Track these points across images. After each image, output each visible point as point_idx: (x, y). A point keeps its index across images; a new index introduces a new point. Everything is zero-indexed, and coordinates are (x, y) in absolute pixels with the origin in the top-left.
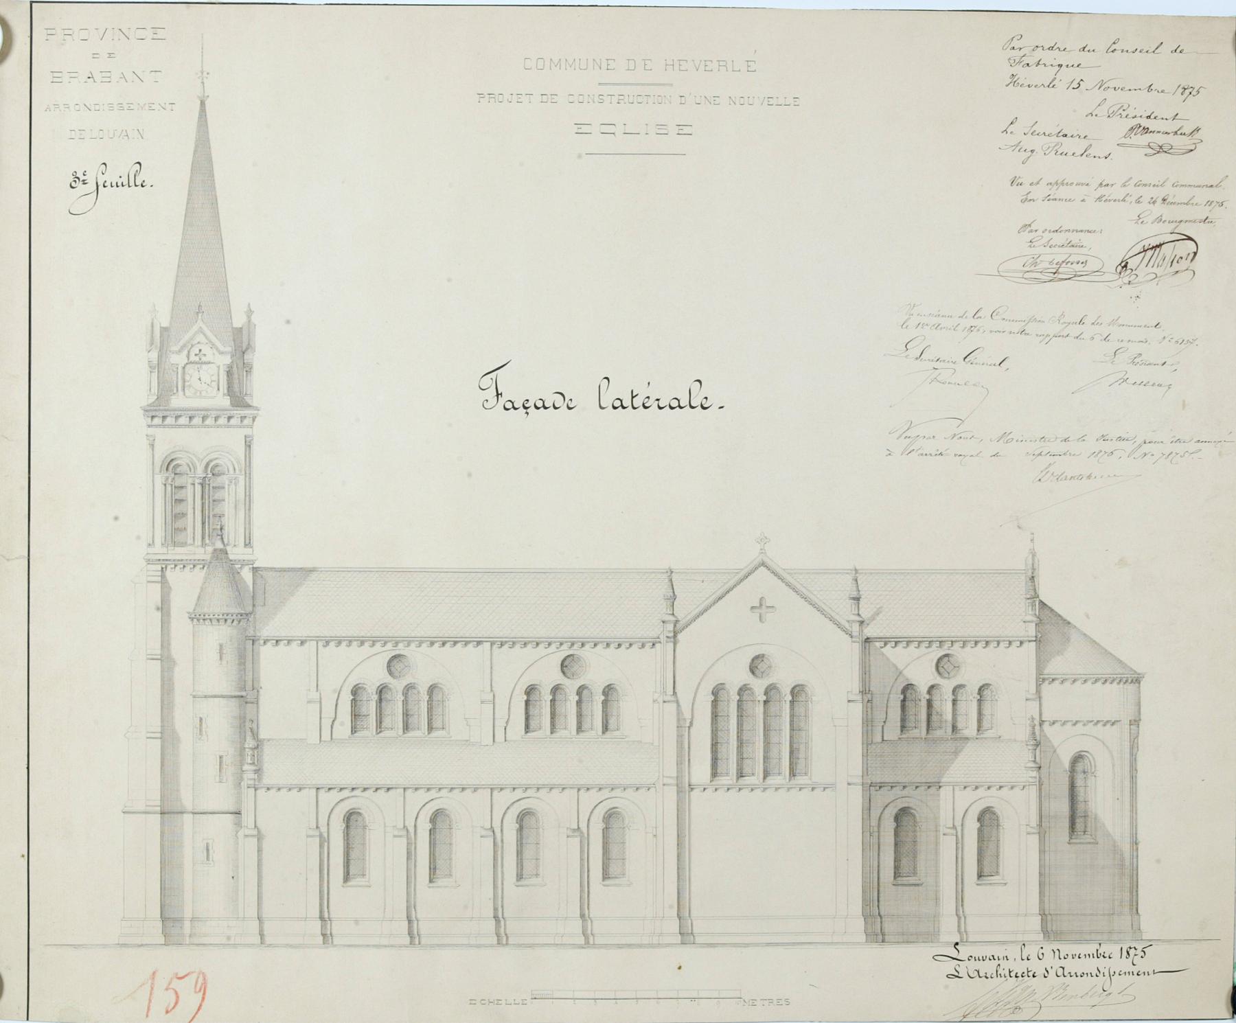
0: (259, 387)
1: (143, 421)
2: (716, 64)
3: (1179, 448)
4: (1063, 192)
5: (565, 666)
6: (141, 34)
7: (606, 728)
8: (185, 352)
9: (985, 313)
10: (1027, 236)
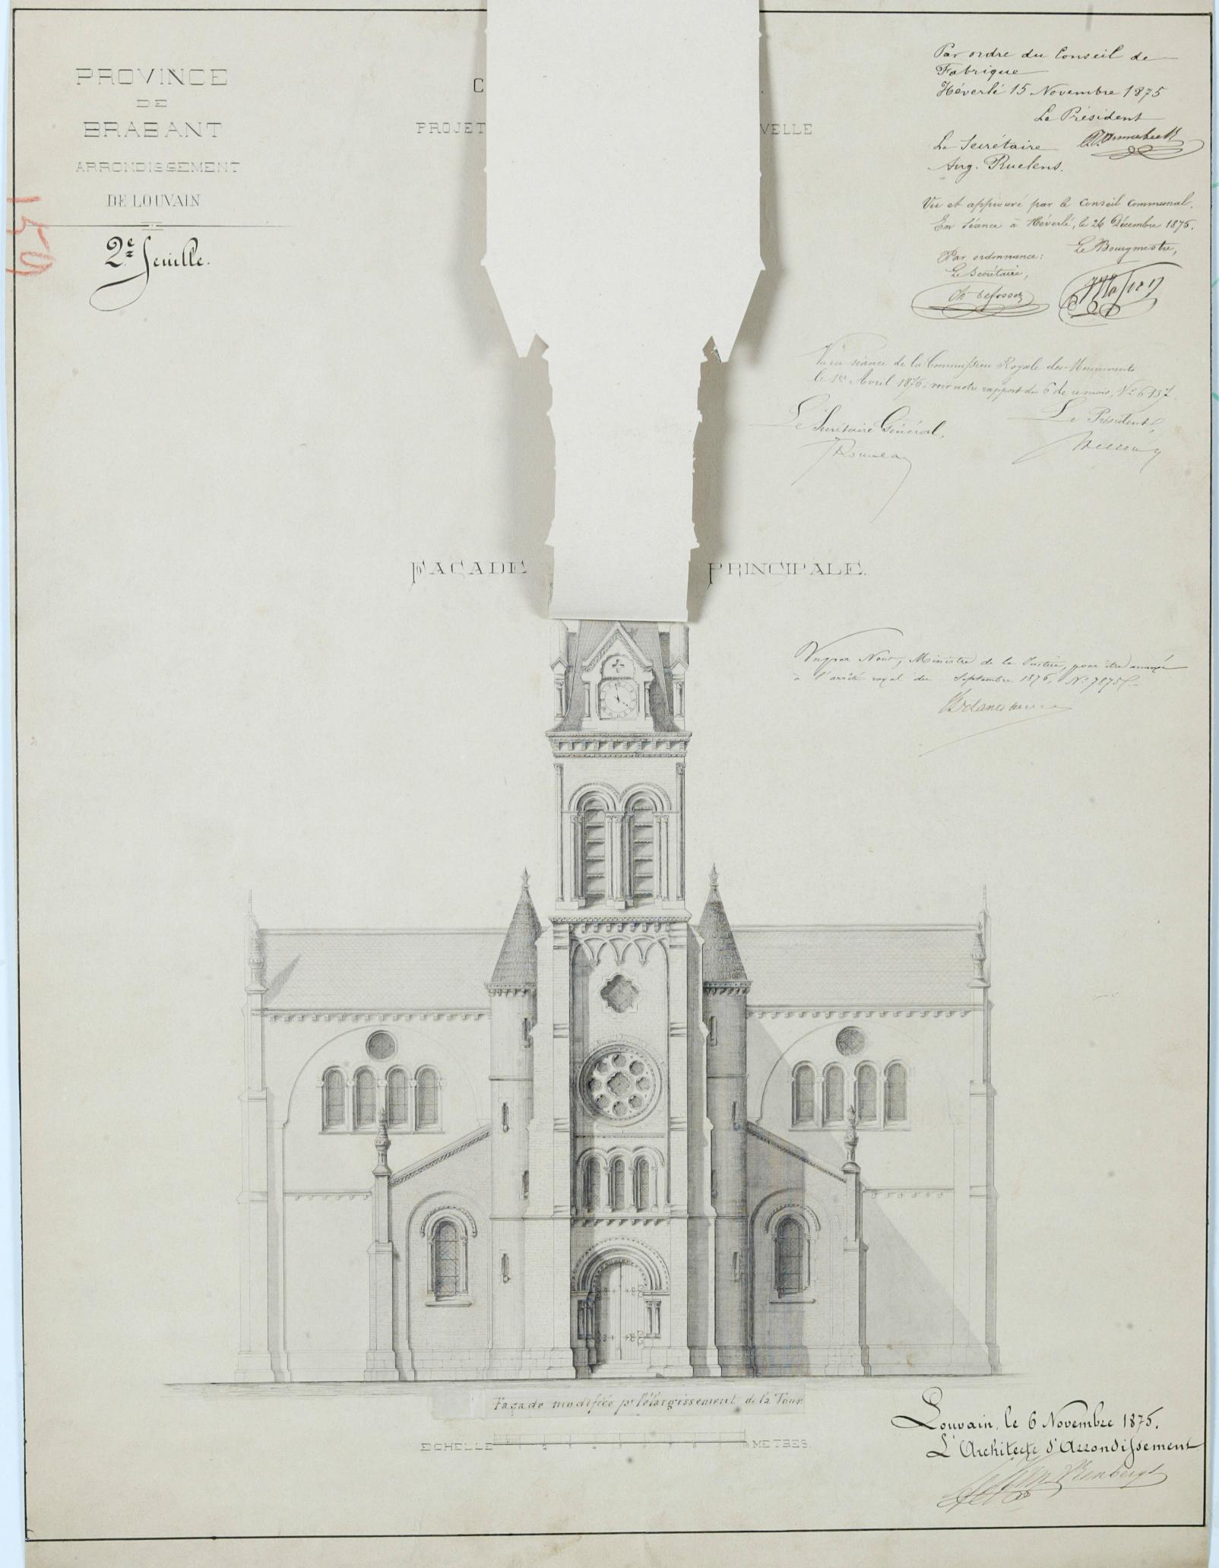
0: (694, 712)
1: (548, 748)
3: (1113, 673)
4: (989, 215)
5: (846, 1039)
6: (197, 77)
7: (888, 1115)
8: (599, 665)
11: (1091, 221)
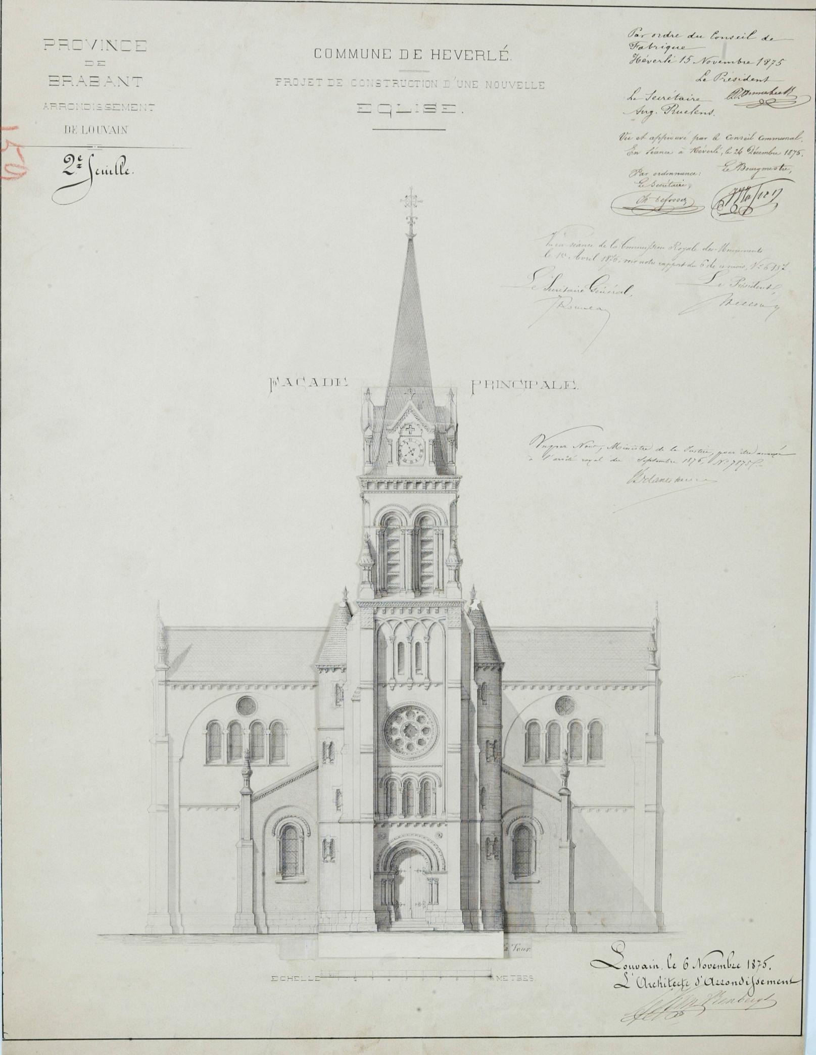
2: (474, 55)
4: (664, 145)
6: (126, 46)
9: (608, 244)
10: (638, 178)
11: (733, 150)
